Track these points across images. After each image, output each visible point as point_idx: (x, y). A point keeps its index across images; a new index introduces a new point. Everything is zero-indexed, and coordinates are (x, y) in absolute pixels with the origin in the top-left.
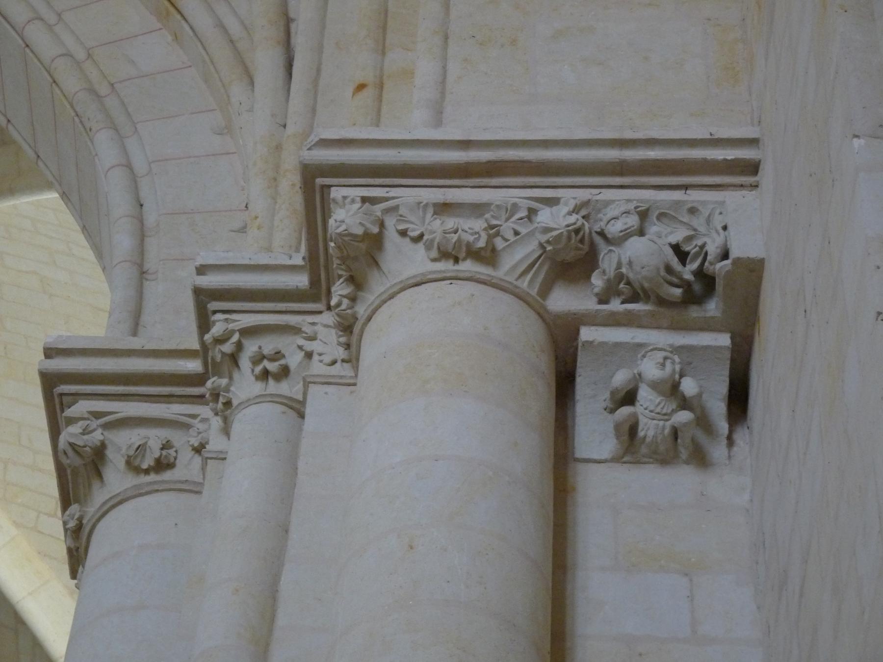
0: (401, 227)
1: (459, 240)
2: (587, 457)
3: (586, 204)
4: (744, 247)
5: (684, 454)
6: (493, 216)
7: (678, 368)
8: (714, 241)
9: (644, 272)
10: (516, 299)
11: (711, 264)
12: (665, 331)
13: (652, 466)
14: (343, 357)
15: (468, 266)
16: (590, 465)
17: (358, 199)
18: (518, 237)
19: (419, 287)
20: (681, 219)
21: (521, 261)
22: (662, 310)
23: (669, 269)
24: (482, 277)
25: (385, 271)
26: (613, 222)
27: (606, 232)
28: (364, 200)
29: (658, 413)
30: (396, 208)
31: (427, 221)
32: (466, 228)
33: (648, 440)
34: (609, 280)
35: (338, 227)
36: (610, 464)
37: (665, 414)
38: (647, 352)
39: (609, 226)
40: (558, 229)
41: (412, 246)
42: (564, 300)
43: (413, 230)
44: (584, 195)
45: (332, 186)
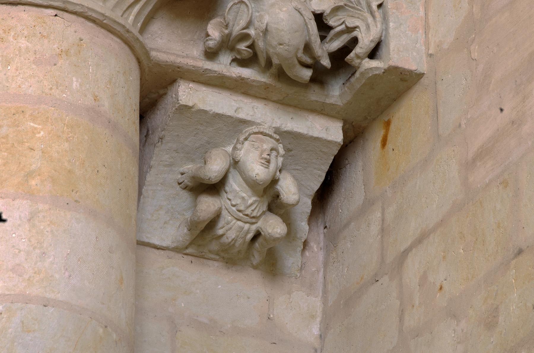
2: (146, 240)
4: (404, 51)
5: (257, 258)
7: (280, 164)
8: (368, 27)
9: (280, 49)
11: (358, 56)
13: (216, 264)
16: (148, 249)
19: (14, 8)
22: (279, 85)
23: (308, 48)
24: (94, 15)
29: (247, 215)
33: (224, 240)
34: (230, 35)
36: (172, 254)
37: (254, 217)
38: (250, 135)
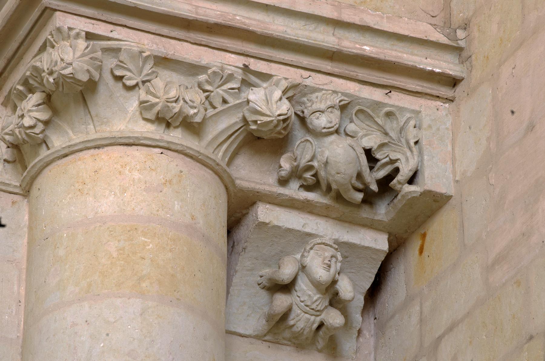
0: (118, 73)
1: (180, 112)
2: (233, 330)
3: (295, 86)
4: (436, 178)
5: (321, 344)
6: (207, 81)
8: (407, 159)
9: (338, 177)
10: (214, 175)
11: (399, 183)
12: (331, 221)
13: (288, 348)
14: (5, 157)
15: (176, 136)
17: (84, 33)
18: (227, 106)
20: (376, 119)
21: (222, 132)
22: (337, 205)
23: (359, 176)
24: (191, 152)
25: (93, 113)
26: (317, 114)
27: (308, 121)
28: (90, 36)
29: (313, 309)
30: (116, 51)
31: (145, 72)
32: (187, 99)
33: (295, 329)
34: (298, 166)
35: (64, 68)
36: (254, 340)
37: (318, 311)
39: (313, 117)
40: (269, 116)
41: (123, 92)
42: (252, 174)
43: (130, 79)
44: (296, 76)
45: (56, 10)
